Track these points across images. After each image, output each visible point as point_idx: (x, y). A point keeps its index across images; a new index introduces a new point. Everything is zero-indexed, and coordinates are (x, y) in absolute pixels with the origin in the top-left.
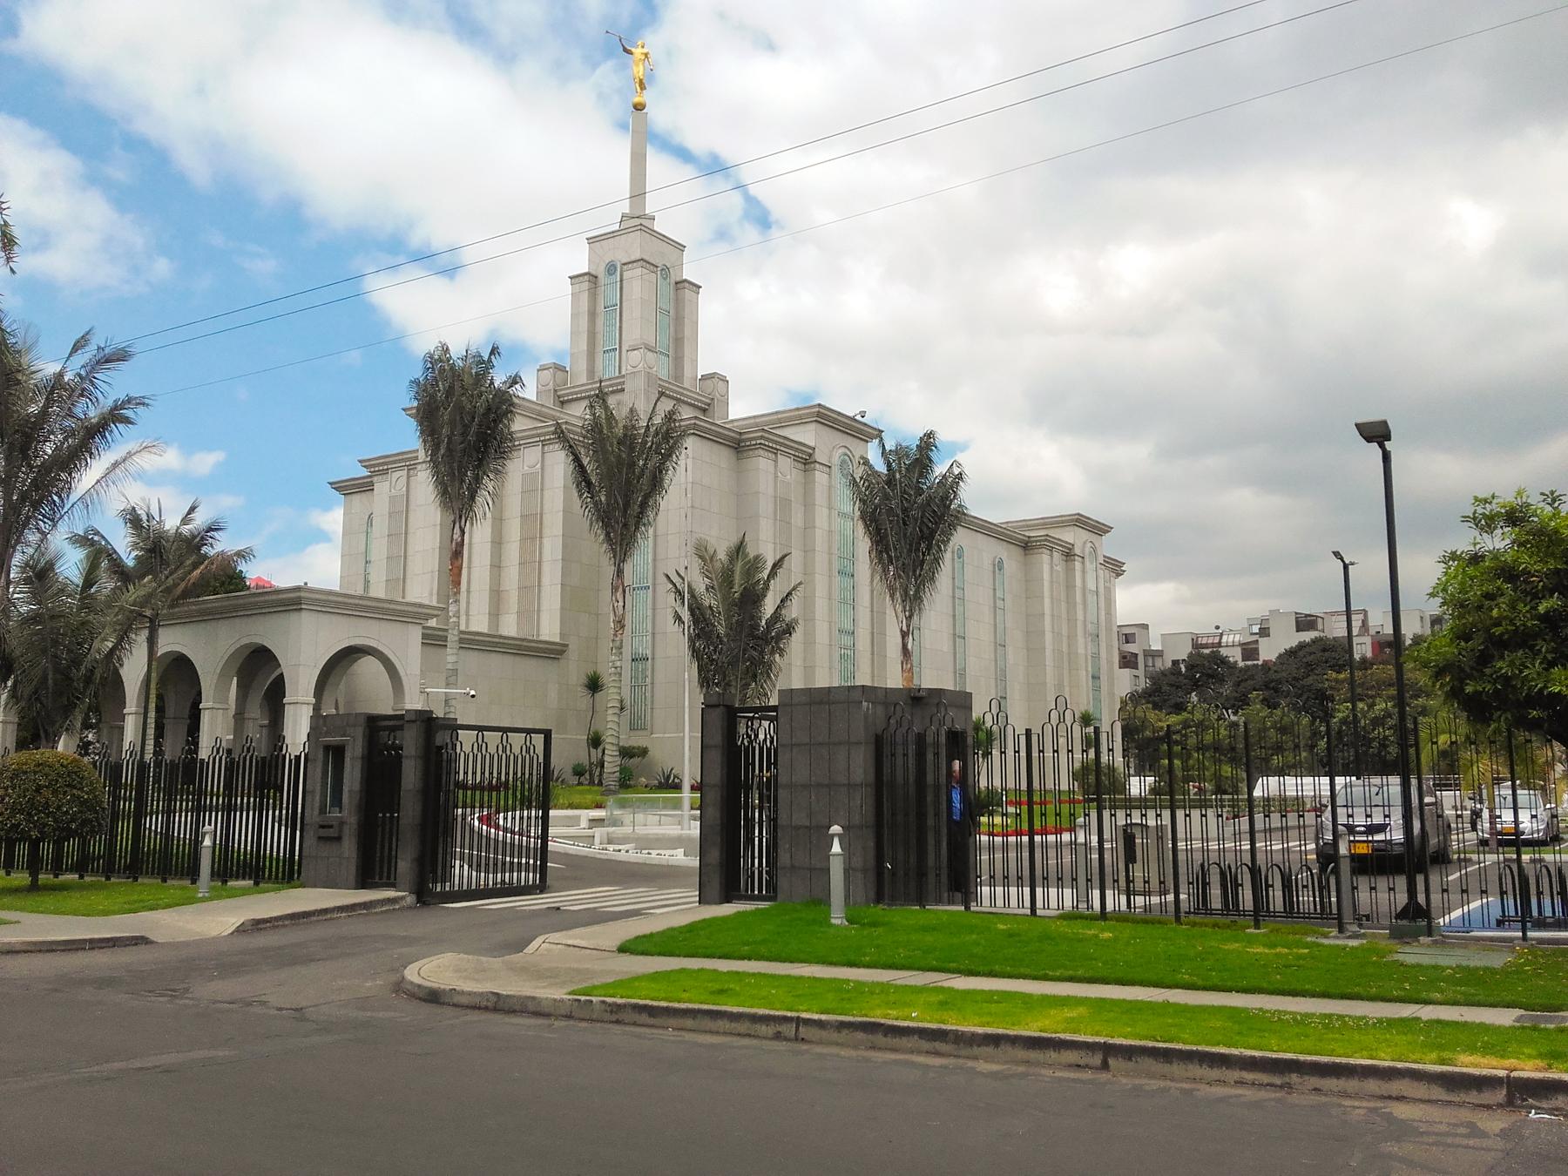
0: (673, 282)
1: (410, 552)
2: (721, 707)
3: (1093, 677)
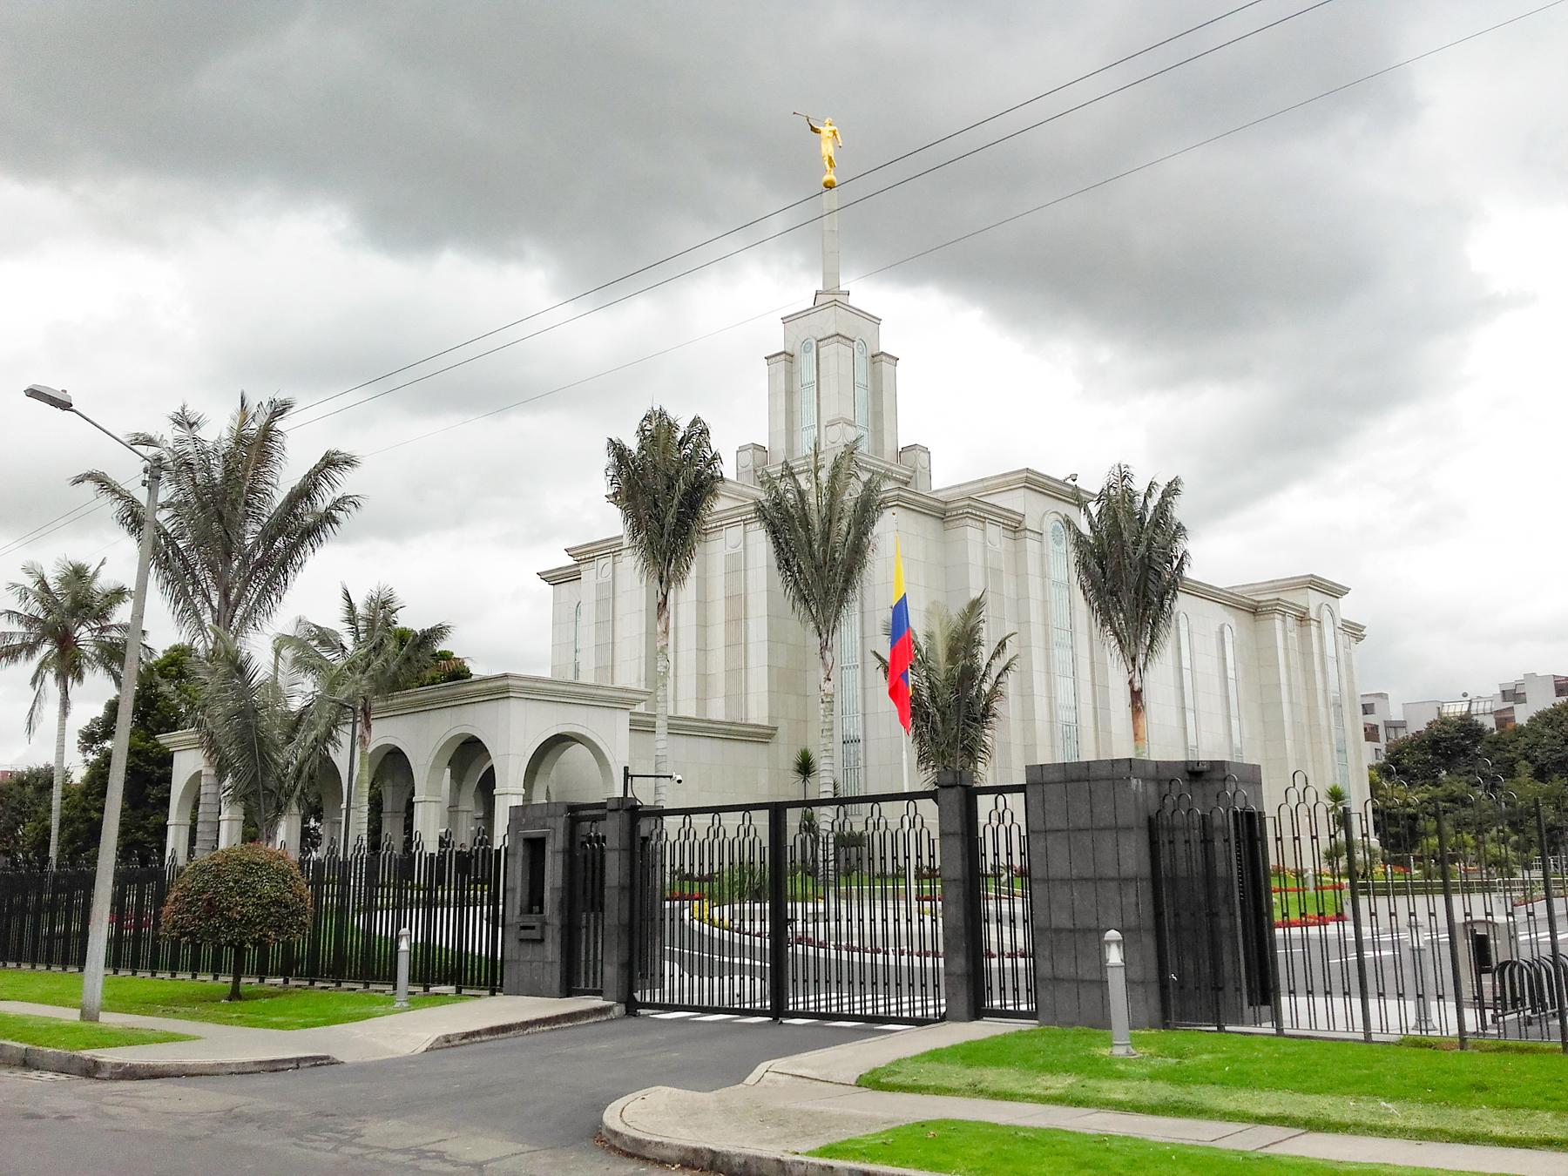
2: (959, 788)
3: (1339, 751)
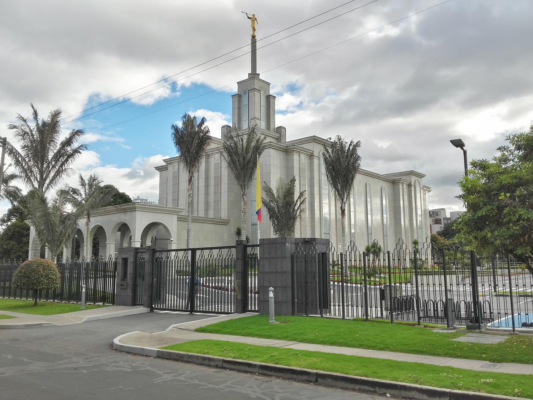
1: (180, 190)
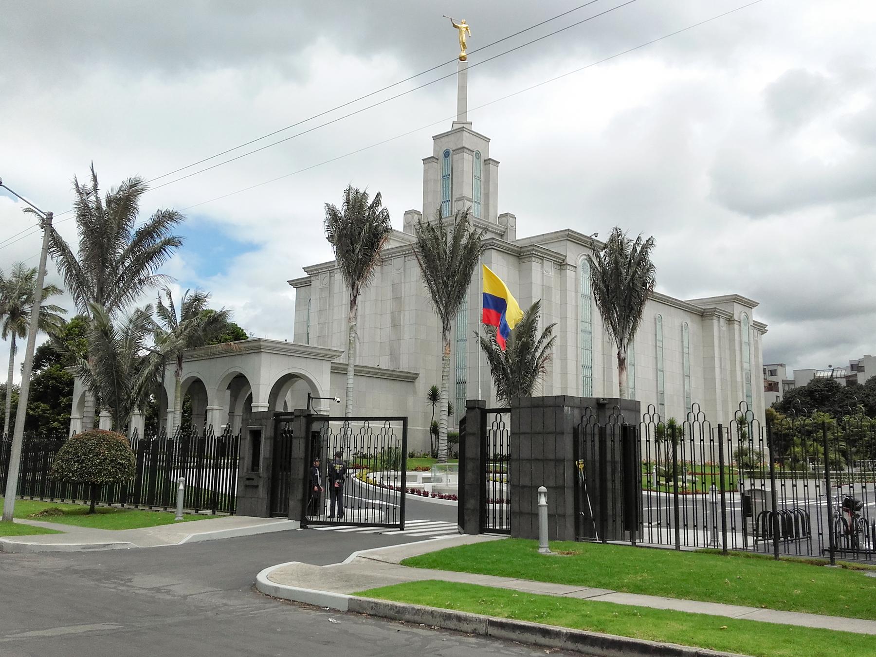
0: (482, 160)
3: (747, 396)
